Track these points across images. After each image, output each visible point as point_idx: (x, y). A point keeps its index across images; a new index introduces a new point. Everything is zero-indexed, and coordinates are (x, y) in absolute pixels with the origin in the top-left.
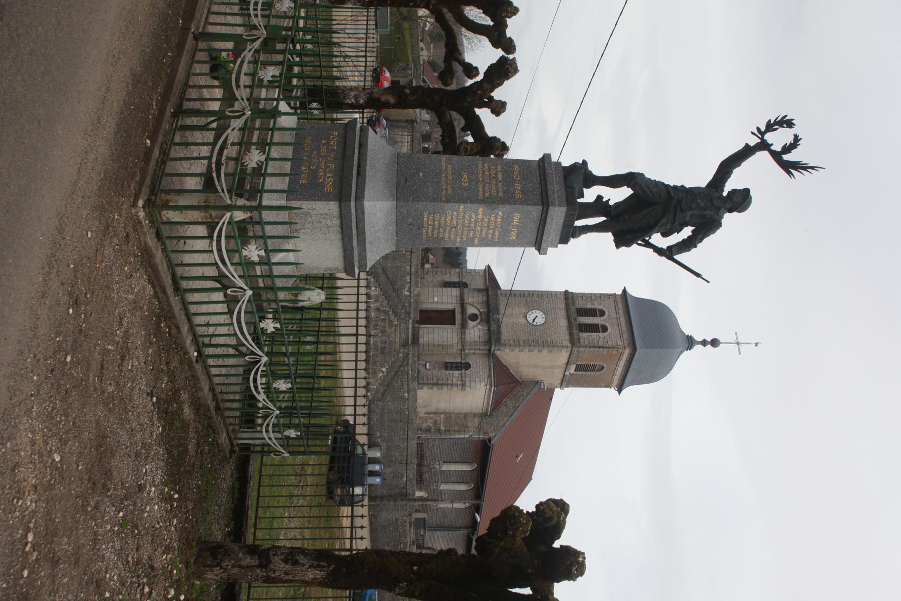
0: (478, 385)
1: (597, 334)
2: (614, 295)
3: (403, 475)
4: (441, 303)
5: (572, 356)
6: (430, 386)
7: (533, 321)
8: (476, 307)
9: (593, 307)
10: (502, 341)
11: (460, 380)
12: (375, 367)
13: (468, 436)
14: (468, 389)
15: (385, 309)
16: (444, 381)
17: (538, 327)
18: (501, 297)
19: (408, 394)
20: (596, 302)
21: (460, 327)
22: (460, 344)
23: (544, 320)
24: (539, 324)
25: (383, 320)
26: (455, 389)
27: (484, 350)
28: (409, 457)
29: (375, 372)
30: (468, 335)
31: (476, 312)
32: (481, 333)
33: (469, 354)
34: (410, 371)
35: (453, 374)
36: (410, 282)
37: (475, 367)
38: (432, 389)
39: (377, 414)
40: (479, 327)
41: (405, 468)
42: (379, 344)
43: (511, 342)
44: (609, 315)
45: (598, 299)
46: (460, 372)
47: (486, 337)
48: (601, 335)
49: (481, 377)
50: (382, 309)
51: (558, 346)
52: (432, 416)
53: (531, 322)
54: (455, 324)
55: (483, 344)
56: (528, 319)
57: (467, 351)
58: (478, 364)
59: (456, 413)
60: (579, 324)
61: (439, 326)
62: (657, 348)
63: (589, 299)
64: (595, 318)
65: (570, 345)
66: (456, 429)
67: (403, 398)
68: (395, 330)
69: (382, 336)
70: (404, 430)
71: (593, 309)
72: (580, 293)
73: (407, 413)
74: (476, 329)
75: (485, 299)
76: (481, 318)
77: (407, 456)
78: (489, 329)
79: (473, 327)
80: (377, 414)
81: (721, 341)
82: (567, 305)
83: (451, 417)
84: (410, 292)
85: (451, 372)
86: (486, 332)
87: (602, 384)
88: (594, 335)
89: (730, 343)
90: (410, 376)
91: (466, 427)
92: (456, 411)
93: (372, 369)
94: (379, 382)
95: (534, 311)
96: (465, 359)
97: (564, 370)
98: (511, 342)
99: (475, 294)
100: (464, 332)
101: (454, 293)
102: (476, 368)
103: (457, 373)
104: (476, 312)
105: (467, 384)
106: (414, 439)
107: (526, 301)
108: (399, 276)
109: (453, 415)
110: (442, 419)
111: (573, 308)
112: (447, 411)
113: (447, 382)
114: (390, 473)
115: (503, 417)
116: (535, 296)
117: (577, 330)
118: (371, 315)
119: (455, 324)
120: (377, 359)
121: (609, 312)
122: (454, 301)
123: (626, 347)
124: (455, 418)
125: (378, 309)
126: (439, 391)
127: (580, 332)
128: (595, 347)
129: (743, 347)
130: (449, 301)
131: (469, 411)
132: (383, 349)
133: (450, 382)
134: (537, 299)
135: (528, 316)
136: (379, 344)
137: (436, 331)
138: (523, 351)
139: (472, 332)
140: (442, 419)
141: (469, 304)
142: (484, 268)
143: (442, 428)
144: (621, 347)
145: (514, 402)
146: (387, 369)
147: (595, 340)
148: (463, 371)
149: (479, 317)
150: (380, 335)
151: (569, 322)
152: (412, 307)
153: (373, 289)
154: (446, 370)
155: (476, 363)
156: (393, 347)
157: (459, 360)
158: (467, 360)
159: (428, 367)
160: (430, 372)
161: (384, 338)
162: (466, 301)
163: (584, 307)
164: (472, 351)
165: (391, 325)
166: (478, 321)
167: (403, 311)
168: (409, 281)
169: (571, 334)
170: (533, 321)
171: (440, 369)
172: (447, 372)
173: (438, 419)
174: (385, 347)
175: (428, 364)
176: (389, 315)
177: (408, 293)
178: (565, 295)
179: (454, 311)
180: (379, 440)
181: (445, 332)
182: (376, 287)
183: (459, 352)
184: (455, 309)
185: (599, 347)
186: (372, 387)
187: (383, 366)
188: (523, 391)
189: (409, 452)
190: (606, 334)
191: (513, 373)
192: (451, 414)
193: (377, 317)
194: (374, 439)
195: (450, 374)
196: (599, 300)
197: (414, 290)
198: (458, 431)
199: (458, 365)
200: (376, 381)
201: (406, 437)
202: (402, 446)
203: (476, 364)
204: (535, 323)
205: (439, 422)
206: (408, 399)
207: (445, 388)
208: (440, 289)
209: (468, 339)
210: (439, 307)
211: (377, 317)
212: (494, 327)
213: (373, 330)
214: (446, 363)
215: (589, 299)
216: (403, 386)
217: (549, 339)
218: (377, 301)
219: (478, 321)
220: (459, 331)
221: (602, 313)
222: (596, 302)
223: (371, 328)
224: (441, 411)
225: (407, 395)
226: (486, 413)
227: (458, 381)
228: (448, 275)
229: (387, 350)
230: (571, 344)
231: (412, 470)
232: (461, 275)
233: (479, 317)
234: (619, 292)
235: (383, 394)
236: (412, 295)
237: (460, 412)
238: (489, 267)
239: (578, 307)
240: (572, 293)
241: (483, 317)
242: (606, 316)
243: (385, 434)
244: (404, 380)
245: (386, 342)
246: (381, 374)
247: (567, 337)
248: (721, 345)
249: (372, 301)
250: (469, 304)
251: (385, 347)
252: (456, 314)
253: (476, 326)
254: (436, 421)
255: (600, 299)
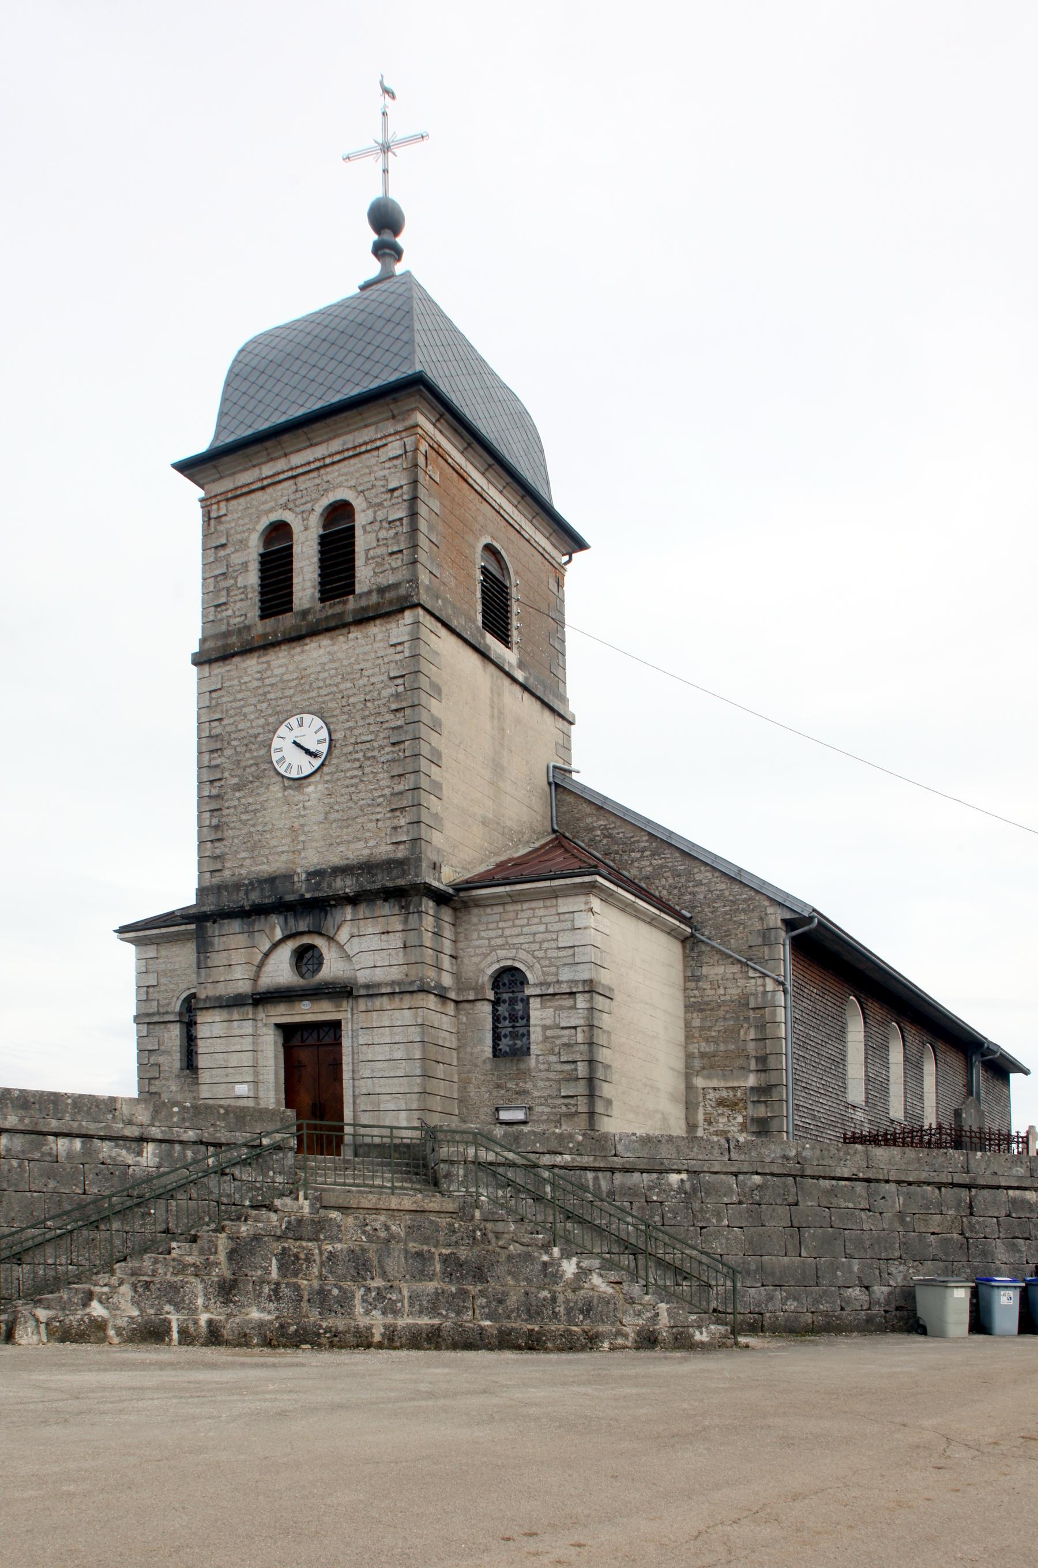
0: (591, 937)
1: (358, 532)
2: (206, 503)
3: (1013, 1201)
4: (256, 1074)
5: (454, 624)
6: (600, 1108)
7: (314, 755)
8: (267, 955)
9: (254, 567)
10: (401, 853)
11: (568, 1002)
12: (561, 1309)
13: (780, 998)
14: (605, 978)
15: (222, 1257)
16: (578, 1057)
17: (338, 736)
18: (227, 873)
19: (669, 1171)
20: (237, 559)
21: (346, 1005)
22: (421, 1000)
23: (307, 718)
24: (324, 734)
25: (289, 1264)
26: (605, 1021)
27: (437, 918)
28: (944, 1178)
29: (587, 1310)
30: (379, 975)
31: (285, 954)
32: (369, 927)
33: (457, 976)
34: (558, 1160)
35: (545, 1028)
36: (86, 1137)
37: (512, 953)
38: (609, 1102)
39: (770, 1298)
40: (343, 936)
41: (985, 1192)
42: (431, 1286)
43: (402, 822)
44: (285, 507)
45: (222, 553)
46: (534, 1003)
47: (385, 908)
48: (361, 519)
49: (556, 927)
50: (223, 1269)
51: (415, 656)
52: (701, 1117)
53: (317, 762)
54: (336, 1025)
55: (413, 919)
56: (307, 770)
57: (447, 980)
58: (500, 941)
59: (689, 1037)
60: (322, 600)
61: (346, 1075)
62: (410, 328)
63: (223, 584)
64: (296, 550)
65: (408, 614)
66: (752, 1035)
67: (688, 1195)
68: (343, 1209)
69: (384, 1275)
70: (832, 1192)
71: (262, 563)
72: (204, 615)
73: (757, 1179)
74: (352, 948)
75: (236, 925)
76: (309, 932)
77: (939, 1186)
78: (354, 900)
79: (348, 958)
80: (770, 1298)
81: (379, 194)
82: (247, 651)
83: (703, 1055)
84: (142, 1139)
85: (536, 1035)
86: (363, 910)
87: (553, 586)
88: (362, 542)
89: (385, 171)
90: (586, 1160)
91: (743, 1002)
92: (681, 1037)
93: (571, 1321)
94: (636, 1290)
95: (275, 757)
96: (479, 988)
97: (507, 682)
98: (402, 822)
99: (217, 959)
100: (367, 986)
101: (218, 1029)
102: (517, 947)
103: (539, 1014)
104: (285, 952)
105: (586, 976)
106: (867, 1153)
107: (238, 788)
108: (52, 1184)
109: (694, 1048)
110: (715, 1083)
111: (260, 628)
112: (680, 1065)
113: (584, 1048)
114: (1014, 1249)
115: (700, 883)
116: (218, 761)
117: (345, 603)
118: (261, 1325)
119: (336, 1025)
120: (512, 1301)
121: (271, 510)
122: (248, 1027)
123: (409, 423)
124: (707, 1040)
125: (227, 1290)
126: (615, 1077)
127: (353, 592)
128: (414, 530)
129: (398, 130)
130: (247, 1043)
131: (679, 995)
132: (453, 1266)
133: (580, 1037)
134: (229, 752)
135: (294, 774)
136: (431, 1286)
137: (364, 1086)
138: (438, 786)
139: (367, 960)
140: (715, 1083)
141: (255, 980)
142: (131, 948)
143: (751, 1081)
144: (409, 441)
145: (635, 855)
146: (566, 1255)
147: (383, 534)
148: (528, 991)
149: (306, 940)
150: (378, 1283)
151: (314, 632)
152: (223, 1137)
153: (97, 1310)
154: (527, 1052)
155: (493, 949)
156: (444, 1221)
157: (487, 1008)
158: (485, 979)
159: (520, 1115)
160: (538, 1109)
161: (396, 1264)
162: (244, 987)
163: (255, 596)
164: (446, 962)
165: (318, 1228)
166: (319, 942)
167: (246, 1174)
168: (78, 1144)
169: (364, 619)
170: (314, 755)
171: (524, 1074)
172: (533, 1048)
173: (712, 1095)
174: (445, 1260)
175: (504, 1116)
176: (256, 1238)
177: (150, 1148)
178: (210, 662)
179: (288, 1032)
180: (880, 1291)
181: (369, 1054)
182: (90, 1296)
183: (451, 1008)
184: (278, 1026)
185: (413, 515)
186: (664, 1320)
187: (550, 1273)
188: (590, 829)
189: (923, 1176)
190: (358, 503)
191: (523, 851)
192: (689, 1056)
193: (276, 1294)
194: (880, 1309)
195: (546, 1038)
196: (228, 551)
197: (130, 1123)
198: (761, 1026)
199: (502, 1009)
200: (631, 1301)
201: (860, 1187)
202: (899, 1203)
203: (501, 947)
204: (324, 748)
205: (724, 1094)
206: (693, 1173)
207: (604, 1055)
208: (204, 1076)
209: (395, 974)
210: (271, 1078)
211: (276, 1294)
212: (346, 885)
213: (350, 1314)
214: (496, 1052)
215: (223, 584)
216: (632, 1192)
217: (386, 693)
218: (173, 1294)
219: (319, 942)
220: (362, 1004)
221: (279, 531)
222: (237, 559)
223: (339, 1323)
224: (682, 1086)
225: (674, 1178)
226: (684, 941)
227: (574, 1007)
228: (161, 1059)
229: (463, 1253)
230: (401, 610)
231: (995, 1168)
232: (156, 1019)
233: (306, 940)
234: (191, 493)
235: (679, 1272)
236: (156, 1132)
237: (682, 1024)
238: (122, 930)
239: (254, 613)
240: (203, 641)
241: (302, 926)
242: (288, 517)
243: (856, 1268)
244: (604, 1185)
245: (419, 1254)
246: (596, 1280)
247: (375, 629)
248: (392, 195)
249: (175, 1320)
250: (255, 980)
251: (445, 1260)
252: (298, 1019)
253: (341, 947)
254: (721, 1103)
255: (223, 546)
